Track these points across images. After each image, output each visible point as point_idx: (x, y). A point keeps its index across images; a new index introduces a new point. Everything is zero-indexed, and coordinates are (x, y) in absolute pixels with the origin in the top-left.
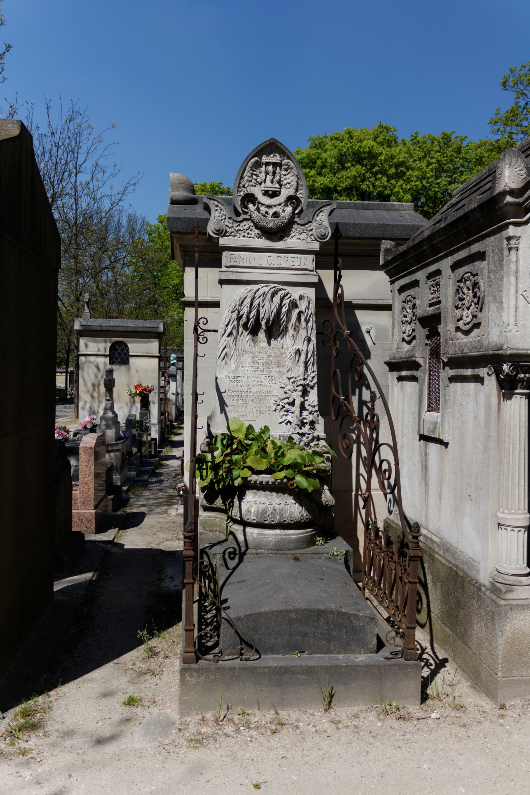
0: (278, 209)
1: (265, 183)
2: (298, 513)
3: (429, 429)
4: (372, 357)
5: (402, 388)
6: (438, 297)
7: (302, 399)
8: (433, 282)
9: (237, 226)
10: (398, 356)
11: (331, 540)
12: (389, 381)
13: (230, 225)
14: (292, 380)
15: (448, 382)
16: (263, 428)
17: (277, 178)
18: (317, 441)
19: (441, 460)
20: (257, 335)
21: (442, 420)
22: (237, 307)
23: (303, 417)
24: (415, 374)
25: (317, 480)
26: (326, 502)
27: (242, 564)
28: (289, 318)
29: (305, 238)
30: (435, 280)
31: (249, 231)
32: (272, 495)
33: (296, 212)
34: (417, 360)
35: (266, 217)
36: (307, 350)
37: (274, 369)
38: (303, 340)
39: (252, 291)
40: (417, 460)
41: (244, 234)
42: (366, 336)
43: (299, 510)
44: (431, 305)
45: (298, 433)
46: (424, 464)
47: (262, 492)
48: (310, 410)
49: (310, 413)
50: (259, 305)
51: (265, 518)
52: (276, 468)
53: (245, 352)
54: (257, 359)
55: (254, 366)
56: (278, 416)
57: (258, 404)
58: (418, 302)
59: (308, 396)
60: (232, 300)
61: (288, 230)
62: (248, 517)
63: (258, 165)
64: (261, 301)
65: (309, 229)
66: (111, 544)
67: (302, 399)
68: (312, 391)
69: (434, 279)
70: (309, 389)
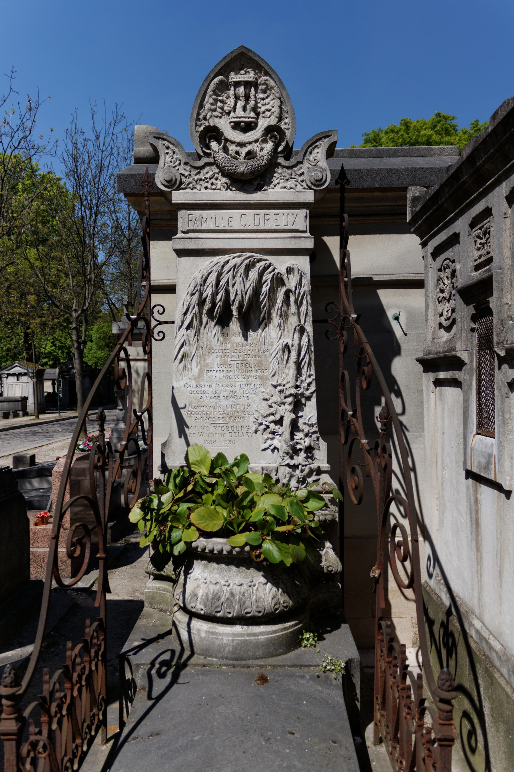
0: (255, 147)
1: (234, 112)
2: (270, 599)
3: (479, 463)
4: (403, 352)
5: (441, 397)
6: (488, 253)
7: (293, 416)
8: (479, 231)
9: (196, 174)
10: (434, 349)
11: (330, 632)
12: (424, 386)
13: (187, 174)
14: (279, 388)
15: (507, 389)
16: (239, 458)
17: (252, 103)
18: (316, 475)
19: (501, 517)
20: (228, 326)
21: (500, 451)
22: (198, 287)
23: (295, 441)
24: (457, 376)
25: (302, 545)
26: (328, 567)
27: (175, 686)
28: (272, 300)
29: (293, 186)
30: (482, 227)
31: (213, 180)
32: (230, 571)
33: (280, 149)
34: (458, 354)
35: (237, 159)
36: (299, 344)
37: (254, 374)
38: (293, 330)
39: (219, 264)
40: (464, 507)
41: (206, 185)
42: (394, 324)
43: (271, 594)
44: (477, 268)
45: (288, 465)
46: (474, 516)
47: (214, 565)
48: (306, 431)
49: (307, 435)
50: (228, 282)
51: (217, 607)
52: (235, 527)
53: (211, 350)
54: (229, 359)
55: (225, 369)
56: (261, 440)
57: (232, 424)
58: (458, 266)
59: (302, 411)
60: (192, 278)
61: (268, 176)
62: (193, 605)
63: (223, 87)
64: (231, 276)
65: (299, 172)
66: (86, 593)
67: (293, 416)
68: (308, 403)
69: (481, 225)
70: (303, 400)
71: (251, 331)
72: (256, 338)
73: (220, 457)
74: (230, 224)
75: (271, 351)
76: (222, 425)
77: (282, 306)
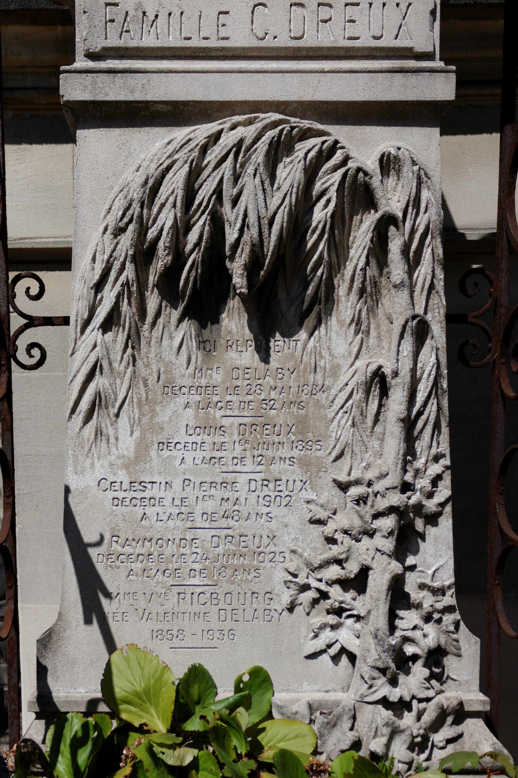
7: (396, 567)
14: (355, 491)
16: (246, 678)
20: (216, 320)
22: (136, 209)
28: (339, 248)
37: (285, 452)
39: (192, 145)
45: (384, 702)
49: (428, 619)
53: (171, 388)
54: (219, 414)
55: (208, 439)
56: (304, 630)
57: (226, 587)
60: (117, 189)
64: (228, 175)
68: (431, 532)
70: (419, 524)
71: (278, 336)
72: (293, 355)
73: (197, 679)
74: (223, 33)
75: (333, 392)
76: (199, 590)
77: (367, 263)
